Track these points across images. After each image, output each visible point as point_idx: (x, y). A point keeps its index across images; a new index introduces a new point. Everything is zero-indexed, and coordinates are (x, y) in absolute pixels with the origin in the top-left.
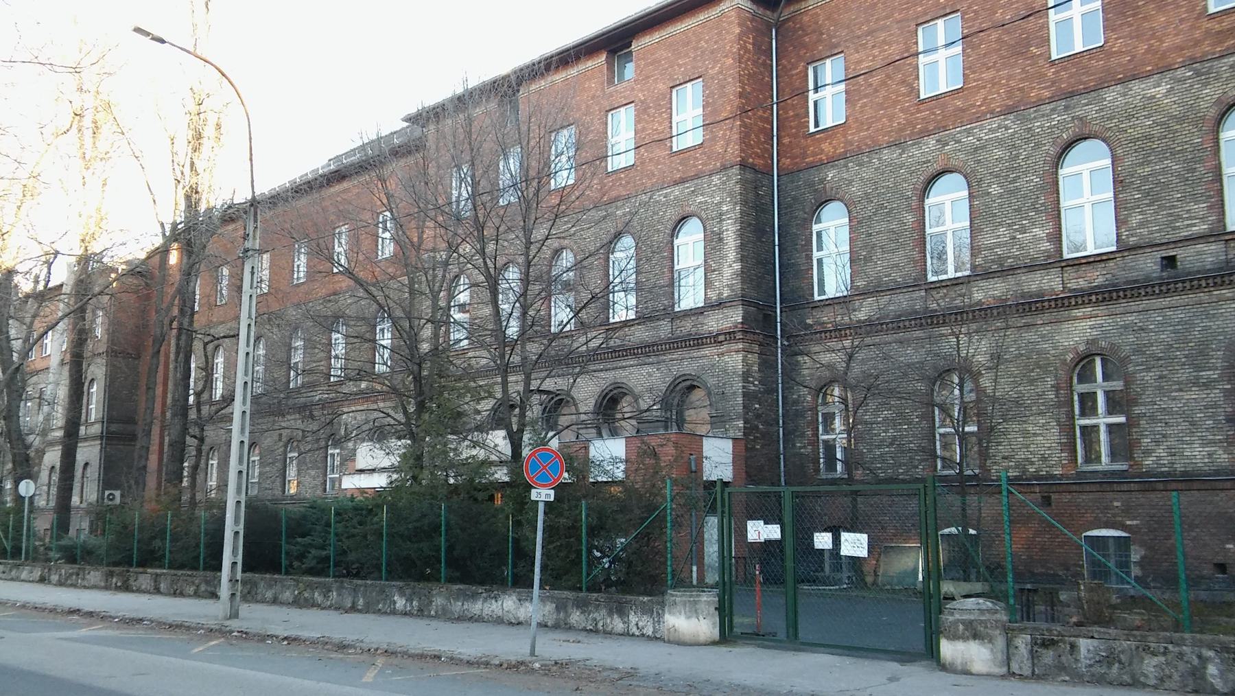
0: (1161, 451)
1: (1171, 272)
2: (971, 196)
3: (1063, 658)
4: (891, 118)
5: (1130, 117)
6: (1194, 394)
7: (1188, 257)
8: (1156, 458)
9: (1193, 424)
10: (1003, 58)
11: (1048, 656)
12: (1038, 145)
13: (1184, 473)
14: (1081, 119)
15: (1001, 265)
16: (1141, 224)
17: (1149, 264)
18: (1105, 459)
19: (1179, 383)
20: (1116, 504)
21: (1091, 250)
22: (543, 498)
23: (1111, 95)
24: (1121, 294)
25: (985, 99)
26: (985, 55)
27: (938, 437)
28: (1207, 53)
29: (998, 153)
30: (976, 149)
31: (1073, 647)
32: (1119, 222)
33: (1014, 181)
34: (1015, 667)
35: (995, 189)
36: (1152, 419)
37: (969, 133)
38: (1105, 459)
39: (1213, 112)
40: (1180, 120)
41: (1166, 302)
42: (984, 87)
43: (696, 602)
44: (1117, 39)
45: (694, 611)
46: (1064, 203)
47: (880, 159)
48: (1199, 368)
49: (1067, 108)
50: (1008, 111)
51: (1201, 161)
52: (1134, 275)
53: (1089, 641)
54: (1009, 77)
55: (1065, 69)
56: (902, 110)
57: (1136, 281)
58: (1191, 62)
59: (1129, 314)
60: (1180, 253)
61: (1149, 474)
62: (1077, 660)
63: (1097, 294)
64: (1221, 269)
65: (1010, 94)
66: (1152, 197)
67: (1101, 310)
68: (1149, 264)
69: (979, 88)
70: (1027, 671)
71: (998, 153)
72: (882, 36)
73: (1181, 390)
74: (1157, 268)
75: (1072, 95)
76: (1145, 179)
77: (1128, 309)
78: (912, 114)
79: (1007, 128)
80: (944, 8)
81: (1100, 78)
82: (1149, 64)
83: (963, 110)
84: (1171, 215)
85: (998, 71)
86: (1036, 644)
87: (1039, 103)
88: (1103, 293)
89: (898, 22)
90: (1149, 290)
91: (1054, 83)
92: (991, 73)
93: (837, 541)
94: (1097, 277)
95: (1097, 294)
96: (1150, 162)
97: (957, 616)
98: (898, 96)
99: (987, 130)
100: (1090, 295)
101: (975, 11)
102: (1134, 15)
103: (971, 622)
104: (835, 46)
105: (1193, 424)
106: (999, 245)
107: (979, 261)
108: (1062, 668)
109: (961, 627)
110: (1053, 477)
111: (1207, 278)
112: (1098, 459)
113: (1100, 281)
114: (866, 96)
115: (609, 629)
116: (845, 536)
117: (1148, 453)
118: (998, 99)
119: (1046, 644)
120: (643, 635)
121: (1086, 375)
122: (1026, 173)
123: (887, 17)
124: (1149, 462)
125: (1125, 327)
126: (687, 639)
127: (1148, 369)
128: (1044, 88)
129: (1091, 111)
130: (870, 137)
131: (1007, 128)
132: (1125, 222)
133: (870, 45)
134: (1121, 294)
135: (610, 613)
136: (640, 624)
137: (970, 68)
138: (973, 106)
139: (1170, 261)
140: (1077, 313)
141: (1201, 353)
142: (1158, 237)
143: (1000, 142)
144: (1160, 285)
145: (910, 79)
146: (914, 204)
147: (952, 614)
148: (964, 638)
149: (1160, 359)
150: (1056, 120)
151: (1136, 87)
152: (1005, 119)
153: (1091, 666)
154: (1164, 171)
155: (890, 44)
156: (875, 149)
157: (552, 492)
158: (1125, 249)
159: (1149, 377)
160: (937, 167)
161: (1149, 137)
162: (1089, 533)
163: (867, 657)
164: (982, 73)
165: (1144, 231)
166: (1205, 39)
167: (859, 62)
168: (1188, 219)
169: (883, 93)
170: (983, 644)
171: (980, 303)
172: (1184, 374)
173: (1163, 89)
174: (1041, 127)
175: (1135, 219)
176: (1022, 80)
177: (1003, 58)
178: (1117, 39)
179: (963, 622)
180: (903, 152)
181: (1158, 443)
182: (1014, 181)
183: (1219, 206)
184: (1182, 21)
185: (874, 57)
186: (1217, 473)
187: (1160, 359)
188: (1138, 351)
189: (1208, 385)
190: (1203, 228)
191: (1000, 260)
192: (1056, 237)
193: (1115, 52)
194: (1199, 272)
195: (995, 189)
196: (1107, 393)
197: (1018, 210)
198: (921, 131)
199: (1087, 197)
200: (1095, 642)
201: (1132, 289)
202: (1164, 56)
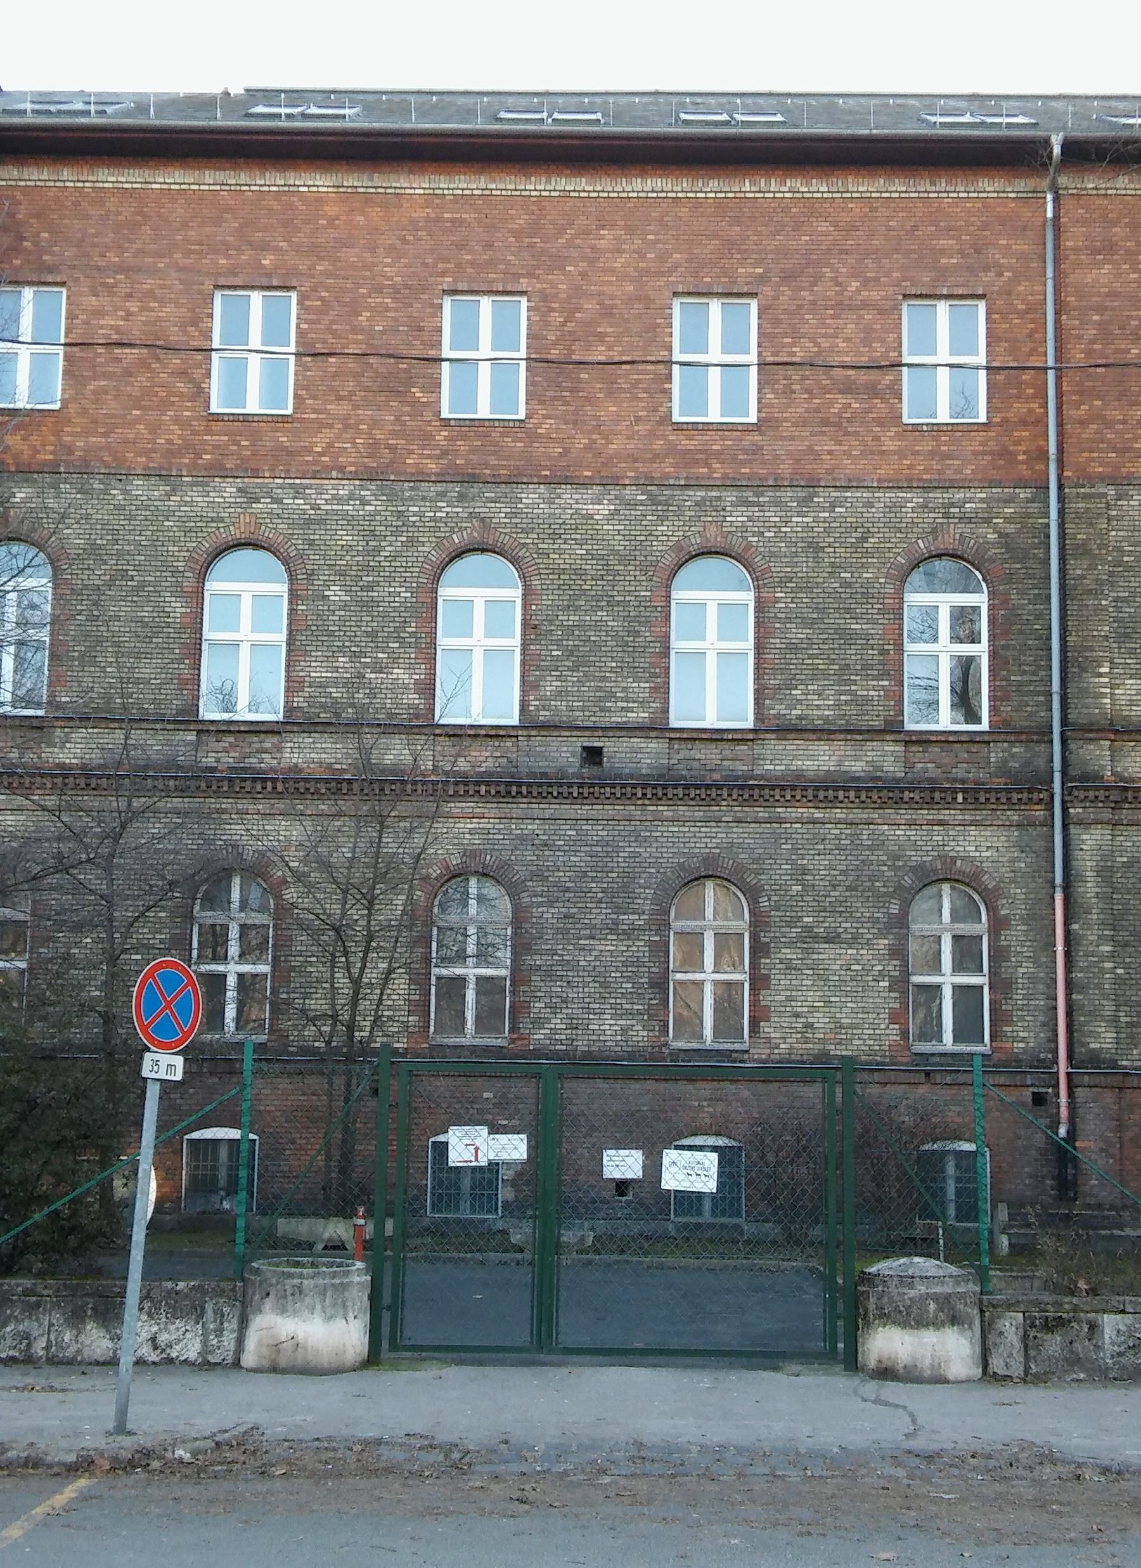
0: (557, 1022)
1: (596, 770)
2: (293, 596)
3: (1077, 1346)
4: (155, 429)
5: (555, 536)
6: (608, 945)
7: (621, 753)
8: (550, 1031)
9: (605, 985)
10: (367, 389)
11: (1054, 1344)
12: (413, 542)
13: (588, 1055)
14: (483, 519)
15: (337, 715)
16: (559, 694)
17: (563, 753)
18: (948, 1036)
19: (593, 927)
20: (486, 1095)
21: (243, 714)
22: (162, 1075)
23: (531, 497)
24: (649, 792)
25: (330, 445)
26: (335, 375)
27: (433, 979)
28: (667, 476)
29: (346, 538)
30: (309, 522)
31: (1093, 1327)
32: (528, 685)
33: (370, 587)
34: (997, 1364)
35: (335, 593)
36: (549, 975)
37: (298, 492)
38: (948, 1036)
39: (669, 560)
40: (625, 560)
41: (584, 811)
42: (331, 426)
43: (344, 1287)
44: (546, 417)
45: (338, 1308)
46: (442, 640)
47: (125, 492)
48: (619, 910)
49: (462, 497)
50: (367, 476)
51: (647, 623)
52: (542, 765)
53: (1119, 1317)
54: (375, 424)
55: (465, 438)
56: (176, 420)
57: (543, 775)
58: (645, 483)
59: (531, 820)
60: (609, 746)
61: (538, 1054)
62: (1097, 1347)
63: (488, 783)
64: (661, 776)
65: (373, 449)
66: (576, 659)
67: (490, 809)
68: (563, 753)
69: (322, 426)
70: (1017, 1370)
71: (346, 538)
72: (149, 283)
73: (592, 937)
74: (576, 761)
75: (472, 479)
76: (570, 630)
77: (530, 813)
78: (195, 433)
79: (364, 502)
80: (269, 276)
81: (517, 467)
82: (588, 468)
83: (291, 453)
84: (600, 689)
85: (356, 407)
86: (1033, 1326)
87: (419, 478)
88: (498, 783)
89: (180, 269)
90: (565, 790)
91: (445, 453)
92: (344, 408)
93: (653, 1168)
94: (483, 759)
95: (488, 783)
96: (577, 609)
97: (922, 1289)
98: (171, 394)
99: (329, 496)
100: (478, 784)
101: (322, 299)
102: (572, 390)
103: (948, 1297)
104: (51, 270)
105: (605, 985)
106: (335, 683)
107: (298, 701)
108: (1074, 1361)
109: (932, 1306)
110: (396, 1052)
111: (644, 787)
112: (460, 1029)
113: (488, 765)
114: (106, 376)
115: (69, 1353)
116: (670, 1156)
117: (539, 1023)
118: (352, 454)
119: (1049, 1326)
120: (170, 1361)
121: (216, 899)
122: (390, 580)
123: (160, 255)
124: (539, 1036)
125: (522, 838)
126: (325, 1361)
127: (551, 903)
128: (430, 457)
129: (500, 512)
130: (108, 447)
131: (364, 502)
132: (535, 686)
133: (123, 289)
134: (524, 790)
135: (76, 1319)
136: (163, 1338)
137: (306, 388)
138: (309, 450)
139: (593, 755)
140: (456, 807)
141: (625, 889)
142: (581, 718)
143: (351, 521)
144: (581, 786)
145: (197, 374)
146: (189, 584)
147: (911, 1286)
148: (936, 1324)
149: (567, 890)
150: (438, 511)
151: (567, 495)
152: (362, 488)
153: (1120, 1354)
154: (597, 626)
155: (162, 302)
156: (120, 474)
157: (179, 1061)
158: (532, 725)
159: (551, 914)
160: (235, 533)
161: (580, 573)
162: (196, 1135)
163: (731, 1367)
164: (326, 402)
165: (562, 706)
166: (667, 456)
167: (99, 313)
168: (622, 700)
169: (142, 380)
170: (960, 1333)
171: (295, 768)
172: (598, 916)
173: (605, 509)
174: (421, 515)
175: (551, 686)
176: (395, 434)
177: (367, 389)
178: (546, 417)
179: (936, 1298)
180: (174, 492)
181: (554, 1009)
182: (370, 587)
183: (662, 690)
184: (638, 419)
185: (129, 314)
186: (631, 1056)
187: (567, 890)
188: (539, 875)
189: (630, 933)
190: (641, 716)
191: (336, 706)
192: (428, 689)
193: (540, 436)
194: (631, 776)
195: (335, 593)
196: (956, 939)
197: (372, 635)
198: (210, 466)
199: (478, 639)
200: (1128, 1319)
201: (540, 785)
202: (609, 462)
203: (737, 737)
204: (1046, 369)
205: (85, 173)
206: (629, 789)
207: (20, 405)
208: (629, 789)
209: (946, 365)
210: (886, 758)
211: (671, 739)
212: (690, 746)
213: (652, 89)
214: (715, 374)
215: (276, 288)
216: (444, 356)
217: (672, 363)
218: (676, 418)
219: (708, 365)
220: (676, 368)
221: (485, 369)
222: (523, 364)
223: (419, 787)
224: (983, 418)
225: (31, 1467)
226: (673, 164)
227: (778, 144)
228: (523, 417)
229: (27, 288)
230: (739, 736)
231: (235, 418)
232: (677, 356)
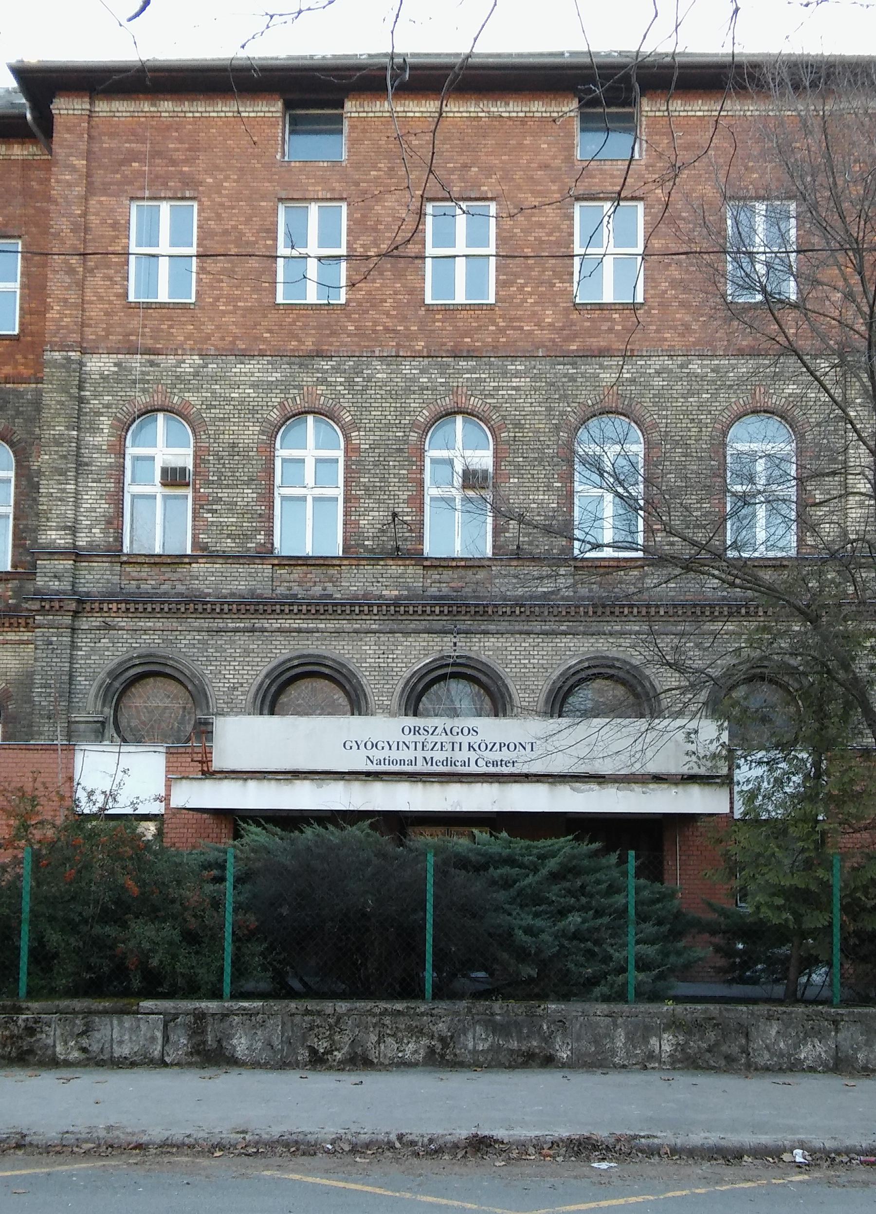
203: (177, 561)
204: (18, 252)
205: (125, 105)
206: (420, 607)
207: (309, 301)
208: (209, 606)
209: (464, 256)
210: (562, 584)
211: (273, 565)
212: (138, 569)
213: (614, 31)
214: (461, 263)
215: (331, 200)
216: (575, 253)
217: (129, 254)
218: (428, 300)
219: (455, 257)
220: (132, 258)
221: (164, 263)
222: (493, 260)
223: (635, 610)
224: (492, 300)
225: (20, 1144)
226: (266, 91)
227: (569, 72)
228: (494, 302)
229: (313, 204)
230: (322, 562)
231: (148, 306)
232: (133, 249)
